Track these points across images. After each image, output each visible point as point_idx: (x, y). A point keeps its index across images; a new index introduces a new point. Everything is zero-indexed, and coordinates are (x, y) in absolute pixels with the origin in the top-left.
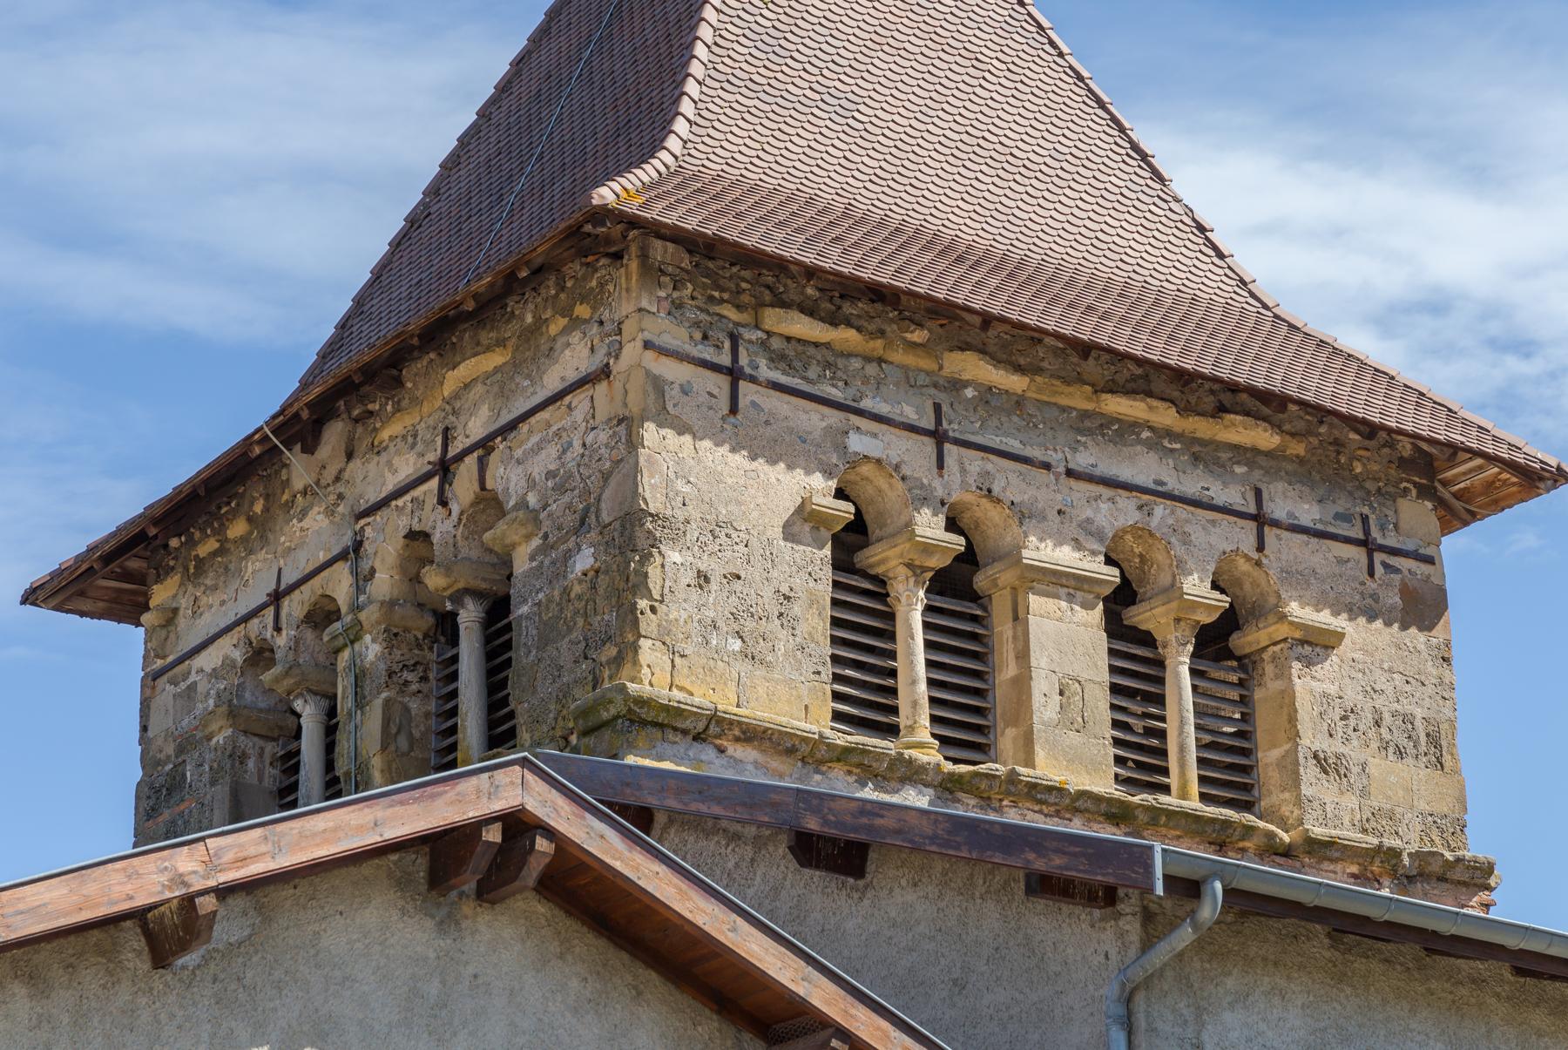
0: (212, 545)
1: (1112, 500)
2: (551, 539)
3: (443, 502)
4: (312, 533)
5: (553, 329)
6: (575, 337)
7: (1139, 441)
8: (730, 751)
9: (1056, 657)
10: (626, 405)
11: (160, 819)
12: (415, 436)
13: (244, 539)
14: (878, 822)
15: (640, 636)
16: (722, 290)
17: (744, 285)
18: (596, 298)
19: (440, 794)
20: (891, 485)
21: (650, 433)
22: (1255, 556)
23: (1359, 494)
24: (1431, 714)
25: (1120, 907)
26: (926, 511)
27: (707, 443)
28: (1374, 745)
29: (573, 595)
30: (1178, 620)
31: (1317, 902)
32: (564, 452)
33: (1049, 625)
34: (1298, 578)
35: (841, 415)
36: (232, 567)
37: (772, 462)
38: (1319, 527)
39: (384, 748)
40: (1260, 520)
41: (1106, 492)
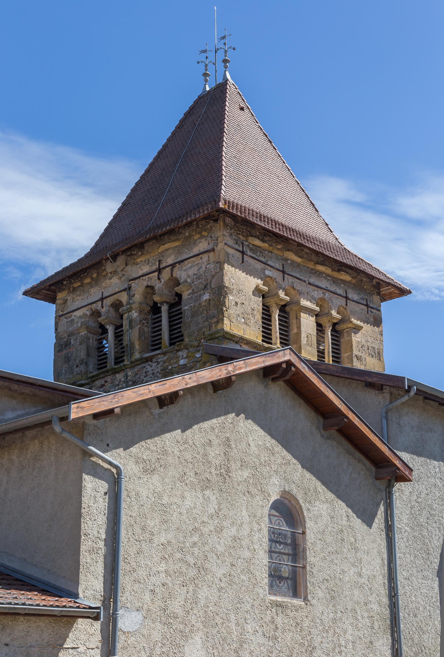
0: (79, 284)
1: (317, 291)
2: (195, 291)
3: (159, 279)
4: (113, 284)
5: (196, 238)
6: (203, 240)
7: (323, 277)
8: (243, 346)
9: (306, 328)
10: (219, 259)
11: (63, 353)
12: (149, 261)
13: (90, 283)
14: (320, 367)
15: (224, 317)
16: (240, 231)
17: (244, 231)
18: (210, 230)
19: (275, 355)
20: (273, 283)
21: (226, 266)
22: (345, 307)
23: (365, 293)
24: (379, 347)
25: (384, 391)
26: (281, 291)
27: (237, 270)
28: (368, 354)
29: (202, 305)
30: (329, 321)
31: (431, 393)
32: (199, 269)
33: (305, 320)
34: (354, 313)
35: (264, 265)
36: (85, 290)
37: (251, 276)
38: (358, 301)
39: (139, 339)
40: (347, 298)
41: (316, 289)
